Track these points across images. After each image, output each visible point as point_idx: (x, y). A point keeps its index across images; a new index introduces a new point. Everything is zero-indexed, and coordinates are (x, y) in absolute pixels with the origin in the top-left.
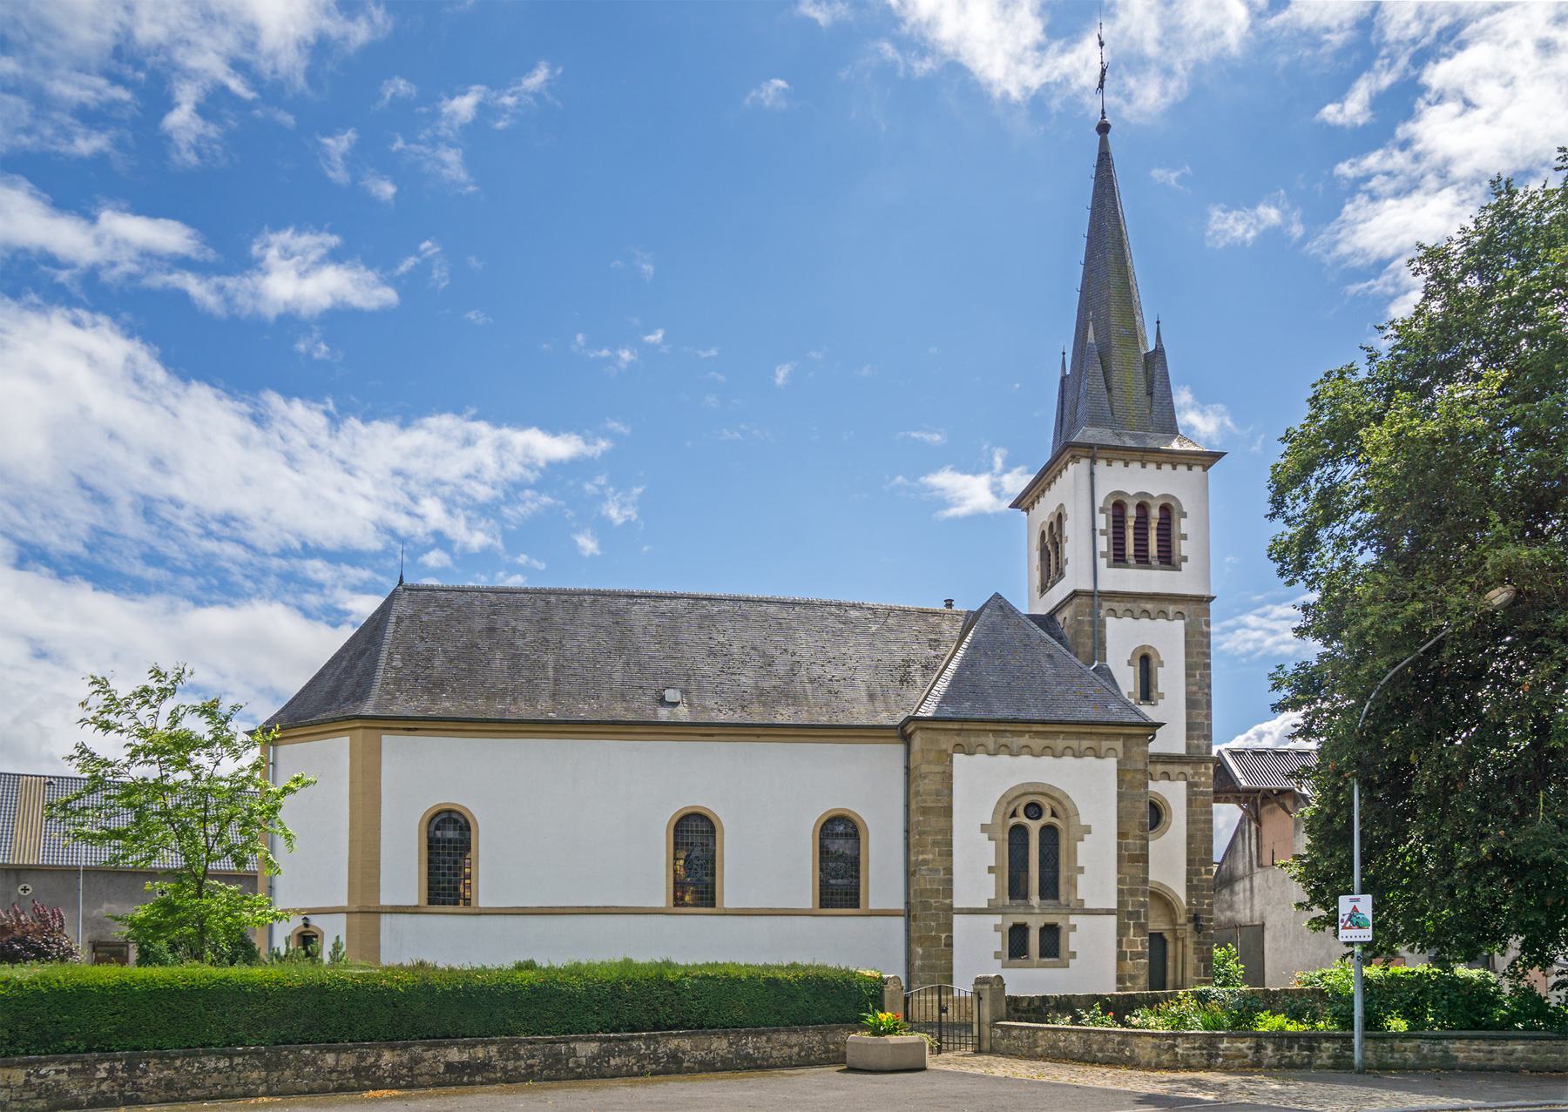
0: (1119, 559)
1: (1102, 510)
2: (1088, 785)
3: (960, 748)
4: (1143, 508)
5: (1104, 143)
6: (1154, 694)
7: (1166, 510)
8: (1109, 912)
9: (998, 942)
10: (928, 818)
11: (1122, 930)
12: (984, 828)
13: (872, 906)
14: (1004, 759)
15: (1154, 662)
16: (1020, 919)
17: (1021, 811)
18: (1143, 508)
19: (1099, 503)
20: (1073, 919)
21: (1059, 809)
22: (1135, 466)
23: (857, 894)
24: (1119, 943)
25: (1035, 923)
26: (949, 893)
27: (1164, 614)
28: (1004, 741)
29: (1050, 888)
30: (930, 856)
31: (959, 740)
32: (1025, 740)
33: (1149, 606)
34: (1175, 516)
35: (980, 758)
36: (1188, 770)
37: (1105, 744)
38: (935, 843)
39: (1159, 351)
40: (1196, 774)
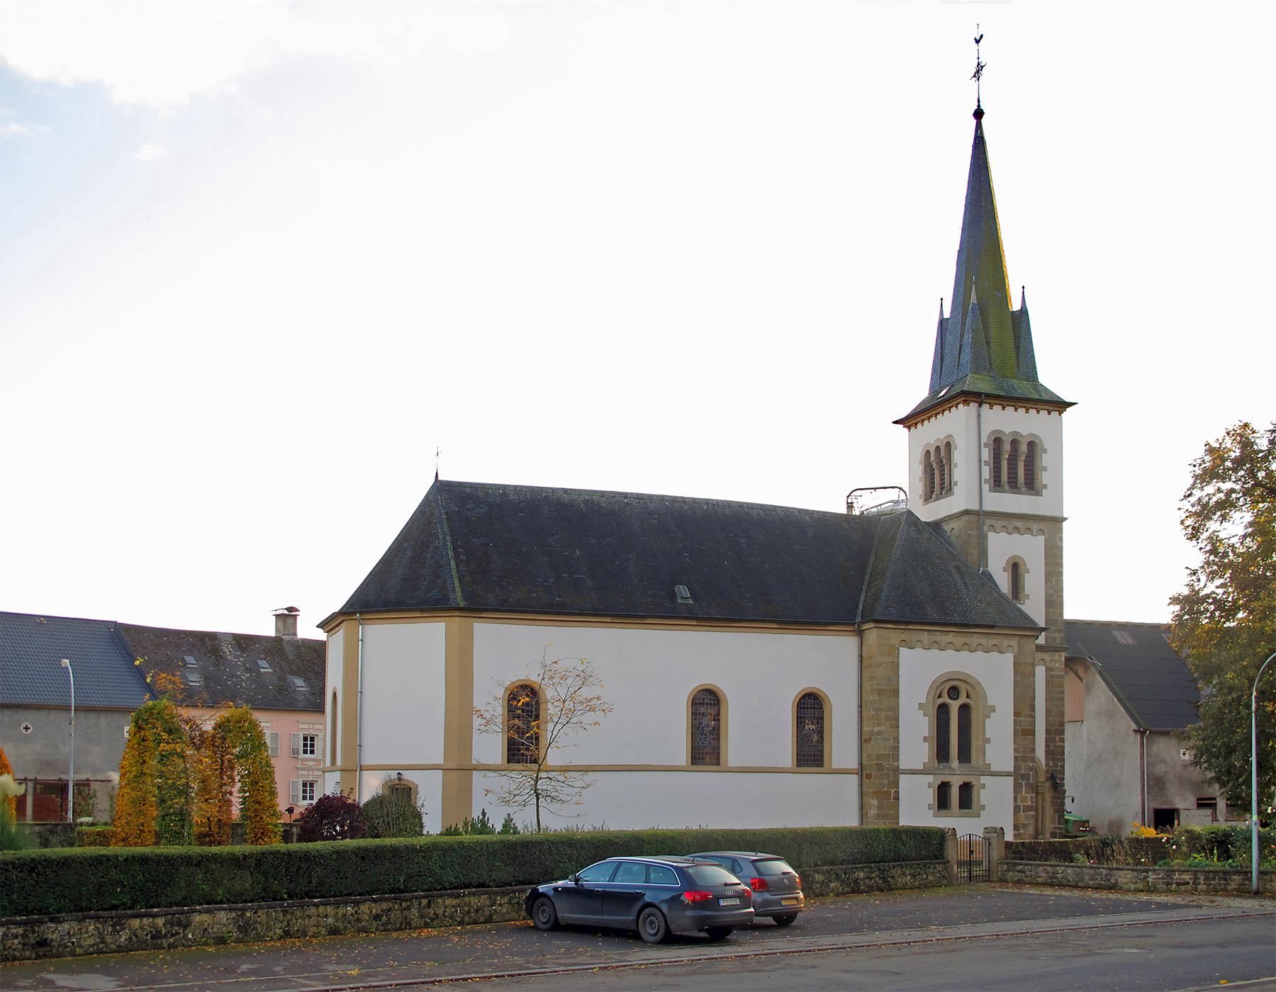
0: (997, 484)
1: (986, 445)
2: (991, 670)
3: (904, 643)
4: (1014, 443)
5: (979, 127)
6: (1021, 595)
7: (1031, 445)
8: (1008, 774)
9: (930, 796)
10: (879, 696)
11: (1017, 788)
12: (921, 706)
13: (835, 766)
14: (935, 652)
15: (1022, 569)
16: (945, 779)
17: (968, 701)
18: (1014, 443)
19: (984, 440)
20: (983, 779)
21: (972, 692)
22: (1010, 410)
23: (822, 756)
24: (1015, 799)
25: (956, 782)
26: (896, 757)
27: (1029, 530)
28: (934, 638)
29: (965, 755)
30: (882, 728)
31: (904, 637)
32: (950, 638)
33: (1019, 524)
34: (1038, 451)
35: (919, 651)
36: (1046, 656)
37: (1006, 642)
38: (887, 718)
39: (1024, 312)
40: (1052, 660)
